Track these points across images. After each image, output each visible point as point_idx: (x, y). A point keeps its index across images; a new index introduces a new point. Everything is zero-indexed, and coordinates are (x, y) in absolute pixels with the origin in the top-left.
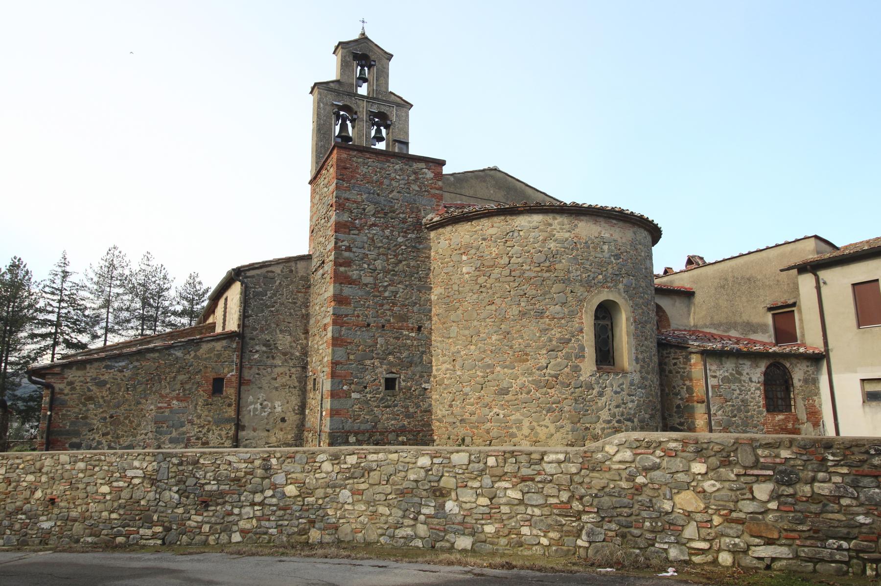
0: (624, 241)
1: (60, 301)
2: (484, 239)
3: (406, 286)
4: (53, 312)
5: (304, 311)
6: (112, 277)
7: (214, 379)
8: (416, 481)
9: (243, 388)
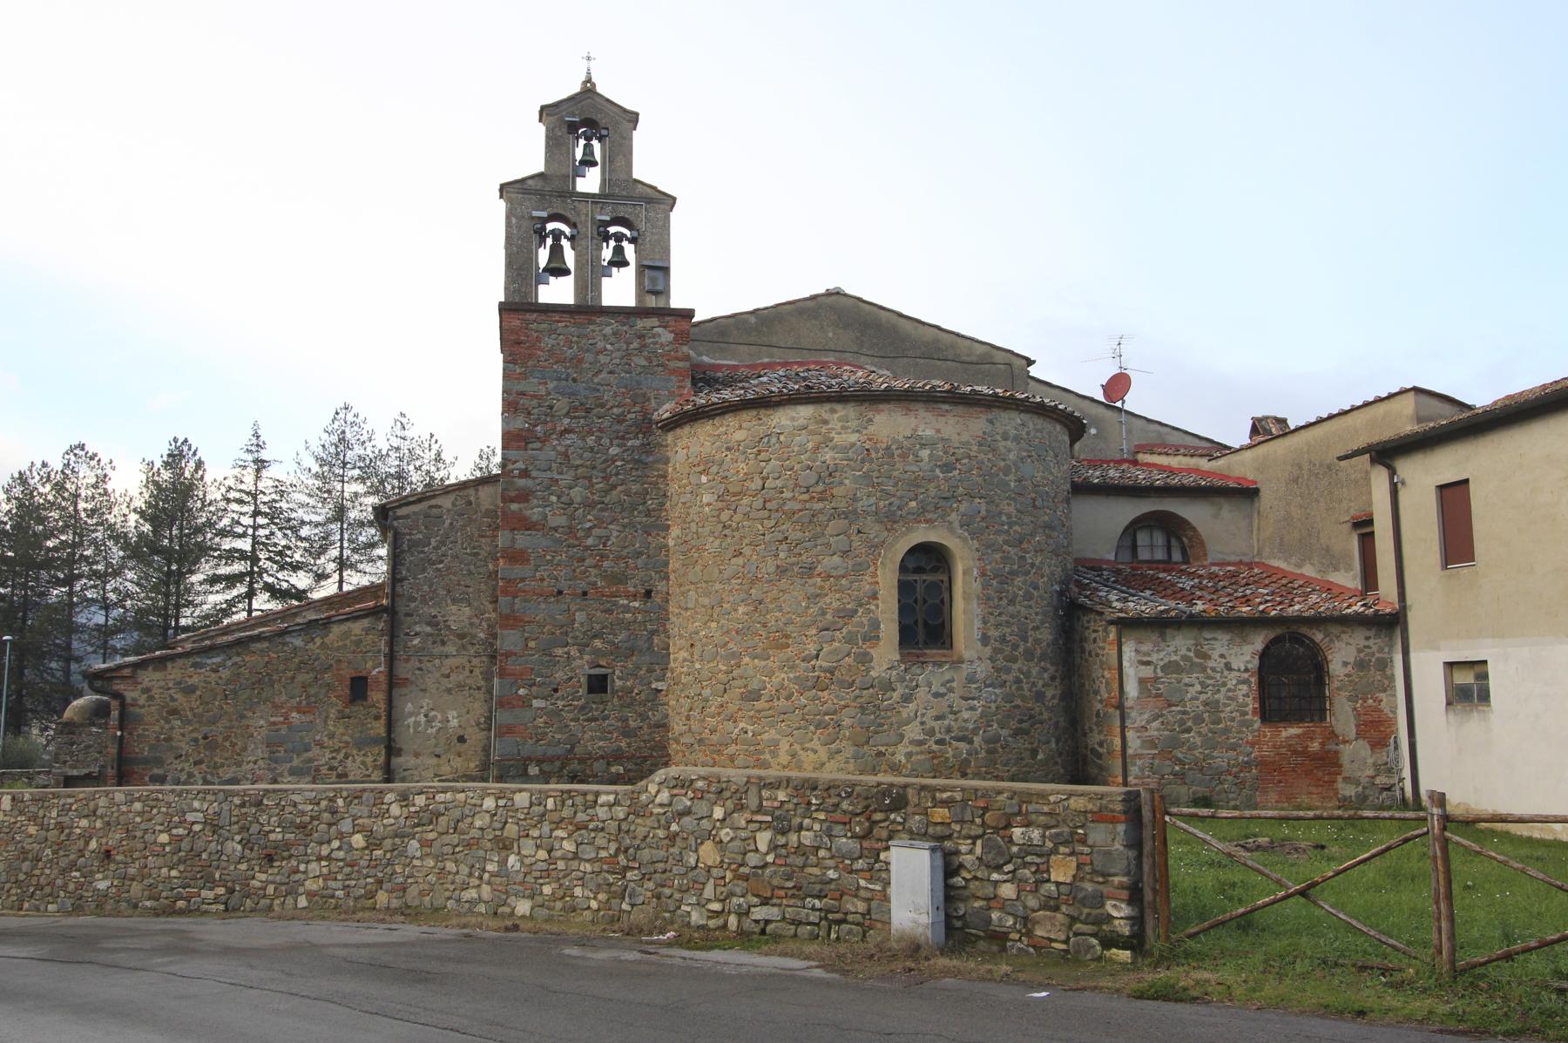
0: (965, 437)
1: (256, 513)
2: (728, 449)
4: (244, 535)
5: (491, 567)
6: (345, 464)
7: (352, 679)
8: (482, 829)
9: (396, 692)
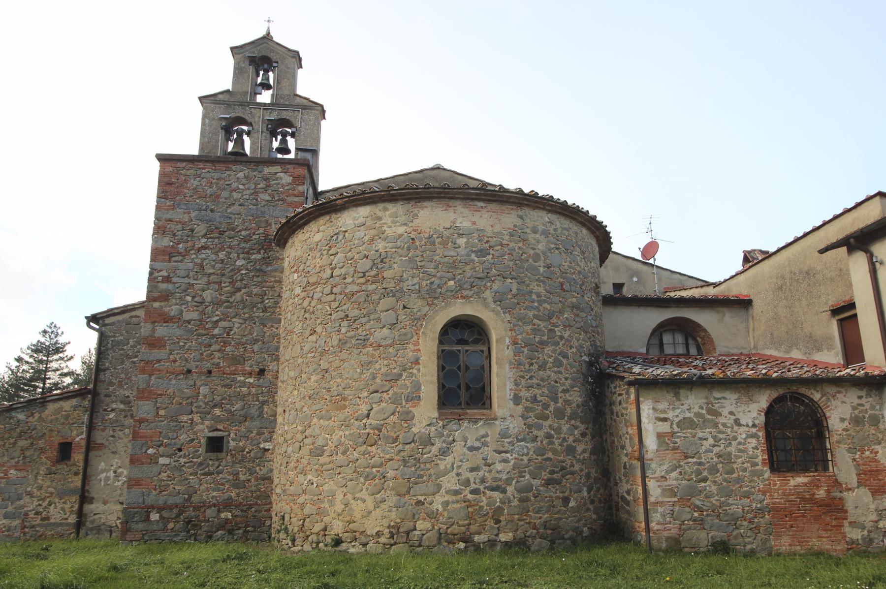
0: (497, 229)
2: (311, 249)
3: (245, 320)
9: (92, 454)
